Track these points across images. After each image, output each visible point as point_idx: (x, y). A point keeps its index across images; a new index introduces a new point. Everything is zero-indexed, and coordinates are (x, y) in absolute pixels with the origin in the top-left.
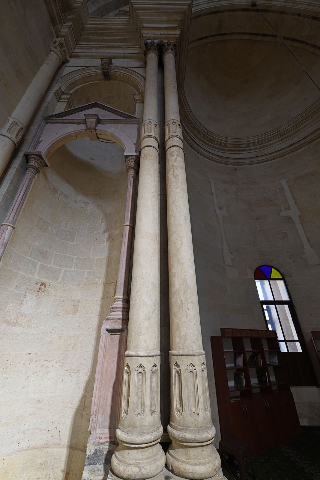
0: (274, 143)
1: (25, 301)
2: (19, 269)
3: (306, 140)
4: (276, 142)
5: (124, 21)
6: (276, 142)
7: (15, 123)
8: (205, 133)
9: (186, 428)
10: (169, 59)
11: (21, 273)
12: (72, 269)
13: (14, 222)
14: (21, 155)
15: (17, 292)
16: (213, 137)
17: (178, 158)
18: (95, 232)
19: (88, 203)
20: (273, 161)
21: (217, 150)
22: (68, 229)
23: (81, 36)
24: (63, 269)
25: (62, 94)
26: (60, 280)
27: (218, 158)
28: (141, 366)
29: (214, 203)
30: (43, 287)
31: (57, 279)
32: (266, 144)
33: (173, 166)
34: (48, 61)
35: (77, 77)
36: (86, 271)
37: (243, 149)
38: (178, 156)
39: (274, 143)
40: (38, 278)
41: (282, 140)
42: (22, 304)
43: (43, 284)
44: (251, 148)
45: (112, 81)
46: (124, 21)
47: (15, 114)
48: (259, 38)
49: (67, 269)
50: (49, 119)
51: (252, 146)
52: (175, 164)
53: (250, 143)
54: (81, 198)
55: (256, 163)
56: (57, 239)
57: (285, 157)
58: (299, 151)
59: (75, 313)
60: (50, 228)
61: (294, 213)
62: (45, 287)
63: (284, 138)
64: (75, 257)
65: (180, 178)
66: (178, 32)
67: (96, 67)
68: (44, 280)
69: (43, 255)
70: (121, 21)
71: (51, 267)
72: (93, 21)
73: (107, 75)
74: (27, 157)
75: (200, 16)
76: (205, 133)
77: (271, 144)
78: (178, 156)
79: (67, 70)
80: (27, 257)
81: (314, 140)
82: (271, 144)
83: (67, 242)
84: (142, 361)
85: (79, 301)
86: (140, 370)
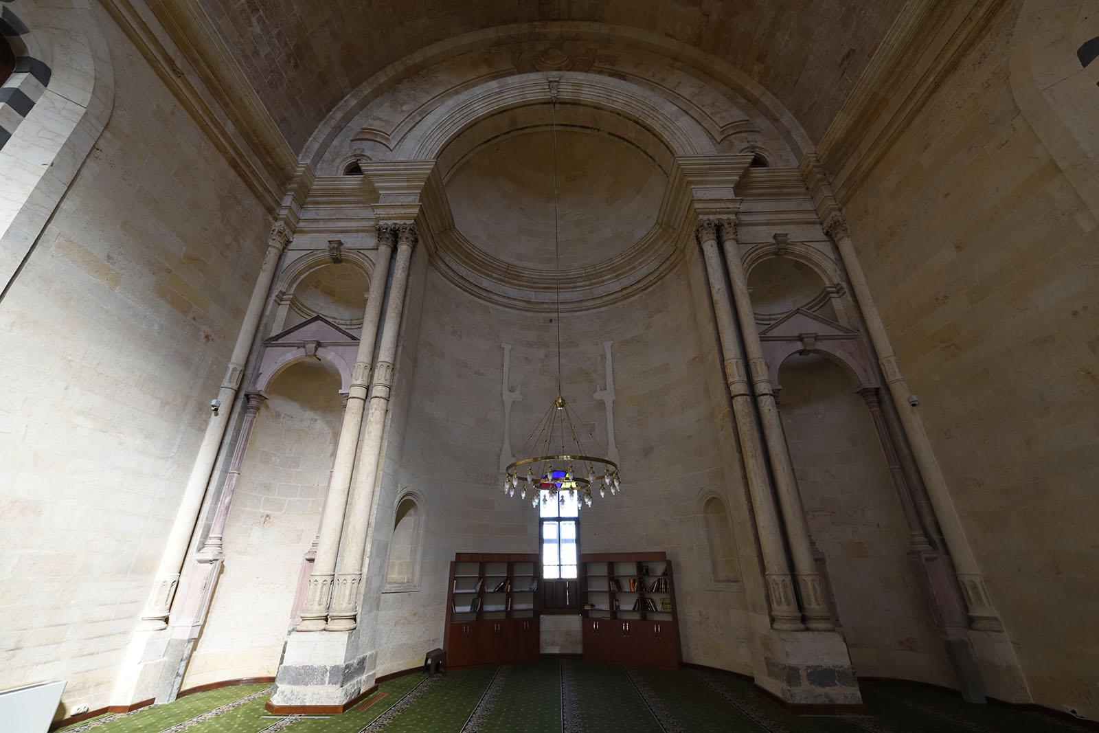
0: (607, 280)
1: (251, 534)
2: (245, 507)
3: (640, 285)
4: (610, 279)
5: (358, 181)
6: (610, 279)
7: (235, 369)
8: (505, 268)
9: (335, 611)
10: (404, 249)
11: (248, 509)
12: (297, 499)
13: (239, 469)
14: (242, 395)
15: (244, 526)
16: (518, 272)
17: (377, 412)
18: (323, 455)
19: (316, 420)
20: (603, 309)
21: (527, 289)
22: (293, 455)
23: (306, 198)
24: (288, 499)
25: (283, 295)
26: (284, 511)
27: (523, 304)
28: (316, 581)
29: (502, 383)
30: (268, 519)
31: (282, 510)
32: (596, 280)
33: (370, 421)
34: (266, 265)
35: (301, 266)
36: (311, 499)
37: (566, 285)
38: (376, 410)
39: (607, 280)
40: (263, 511)
41: (617, 276)
42: (249, 536)
43: (267, 516)
44: (577, 284)
45: (343, 264)
46: (358, 181)
47: (233, 359)
48: (577, 129)
49: (292, 499)
50: (271, 342)
51: (579, 282)
52: (372, 419)
53: (574, 278)
54: (309, 414)
55: (582, 310)
56: (281, 469)
57: (617, 304)
58: (633, 298)
59: (298, 542)
60: (273, 459)
61: (608, 397)
62: (270, 518)
63: (621, 274)
64: (300, 485)
65: (372, 435)
66: (417, 210)
67: (323, 250)
68: (268, 512)
69: (267, 487)
70: (356, 180)
71: (275, 499)
72: (319, 181)
73: (337, 260)
74: (247, 396)
75: (475, 124)
76: (505, 268)
77: (603, 281)
78: (376, 410)
79: (291, 257)
80: (252, 494)
81: (647, 288)
82: (603, 281)
83: (292, 470)
84: (316, 578)
85: (303, 530)
86: (316, 583)
